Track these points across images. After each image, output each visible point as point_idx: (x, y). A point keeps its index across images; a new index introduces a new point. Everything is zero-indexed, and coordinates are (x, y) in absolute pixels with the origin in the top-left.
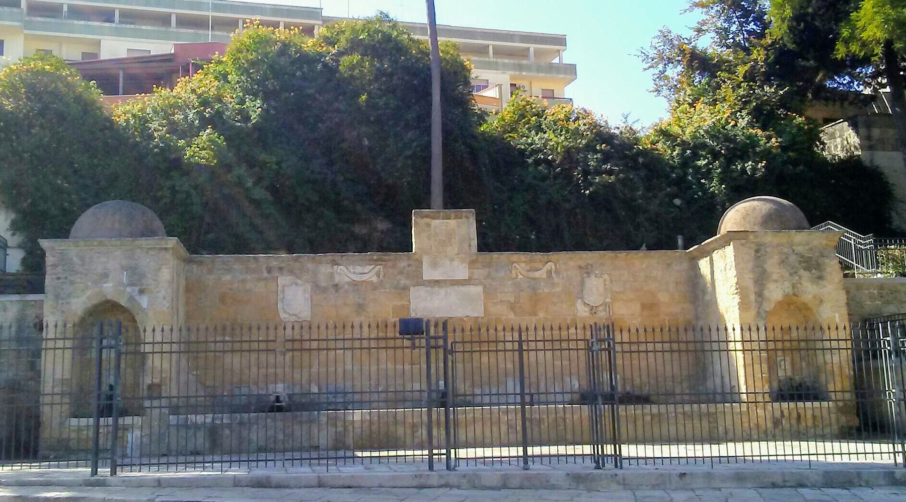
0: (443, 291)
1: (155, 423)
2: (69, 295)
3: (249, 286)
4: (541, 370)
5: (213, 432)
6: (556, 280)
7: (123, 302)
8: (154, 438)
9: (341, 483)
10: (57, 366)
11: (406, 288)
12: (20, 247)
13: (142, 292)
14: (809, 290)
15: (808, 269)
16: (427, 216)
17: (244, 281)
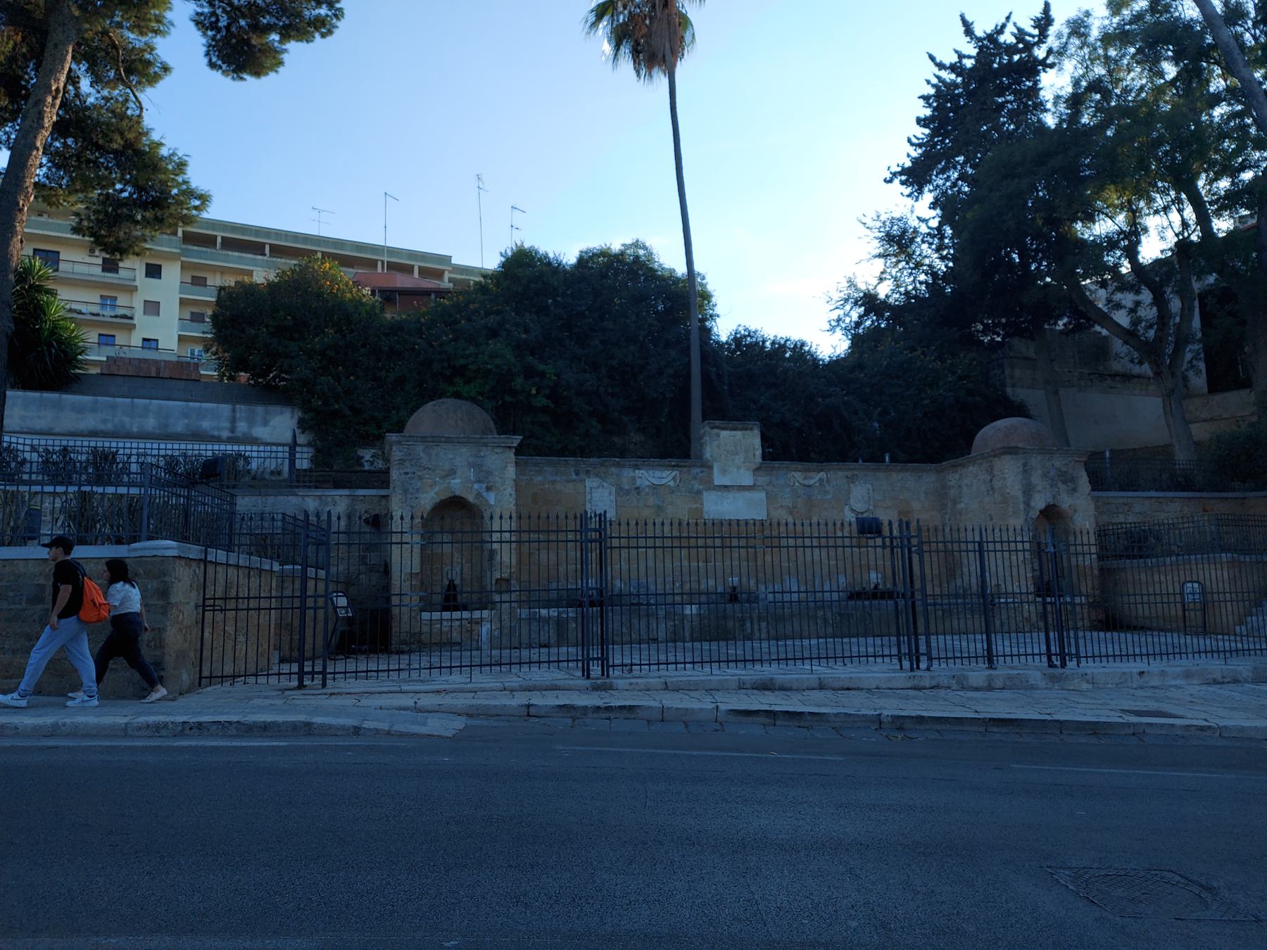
0: (731, 495)
1: (505, 617)
2: (418, 491)
3: (558, 487)
4: (817, 568)
5: (560, 624)
6: (828, 488)
7: (471, 498)
8: (506, 631)
9: (841, 684)
10: (405, 559)
11: (699, 492)
12: (309, 445)
13: (489, 489)
14: (1065, 502)
15: (1065, 482)
16: (717, 427)
17: (553, 482)
